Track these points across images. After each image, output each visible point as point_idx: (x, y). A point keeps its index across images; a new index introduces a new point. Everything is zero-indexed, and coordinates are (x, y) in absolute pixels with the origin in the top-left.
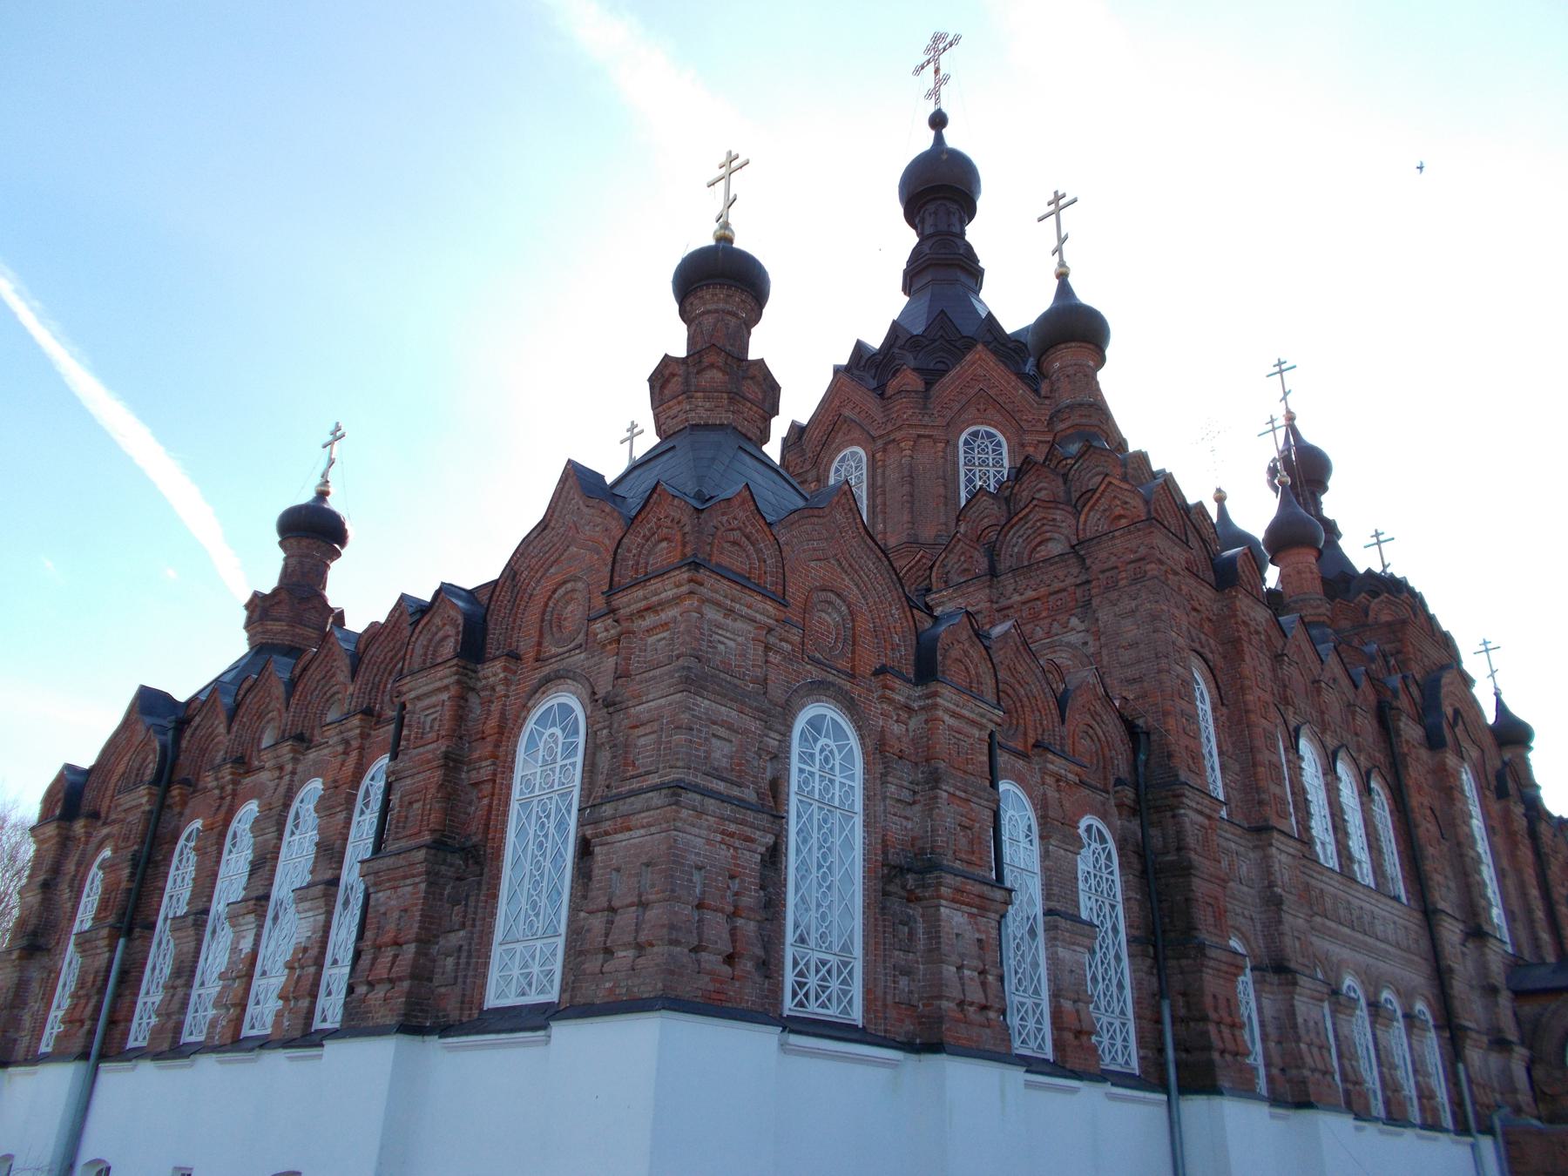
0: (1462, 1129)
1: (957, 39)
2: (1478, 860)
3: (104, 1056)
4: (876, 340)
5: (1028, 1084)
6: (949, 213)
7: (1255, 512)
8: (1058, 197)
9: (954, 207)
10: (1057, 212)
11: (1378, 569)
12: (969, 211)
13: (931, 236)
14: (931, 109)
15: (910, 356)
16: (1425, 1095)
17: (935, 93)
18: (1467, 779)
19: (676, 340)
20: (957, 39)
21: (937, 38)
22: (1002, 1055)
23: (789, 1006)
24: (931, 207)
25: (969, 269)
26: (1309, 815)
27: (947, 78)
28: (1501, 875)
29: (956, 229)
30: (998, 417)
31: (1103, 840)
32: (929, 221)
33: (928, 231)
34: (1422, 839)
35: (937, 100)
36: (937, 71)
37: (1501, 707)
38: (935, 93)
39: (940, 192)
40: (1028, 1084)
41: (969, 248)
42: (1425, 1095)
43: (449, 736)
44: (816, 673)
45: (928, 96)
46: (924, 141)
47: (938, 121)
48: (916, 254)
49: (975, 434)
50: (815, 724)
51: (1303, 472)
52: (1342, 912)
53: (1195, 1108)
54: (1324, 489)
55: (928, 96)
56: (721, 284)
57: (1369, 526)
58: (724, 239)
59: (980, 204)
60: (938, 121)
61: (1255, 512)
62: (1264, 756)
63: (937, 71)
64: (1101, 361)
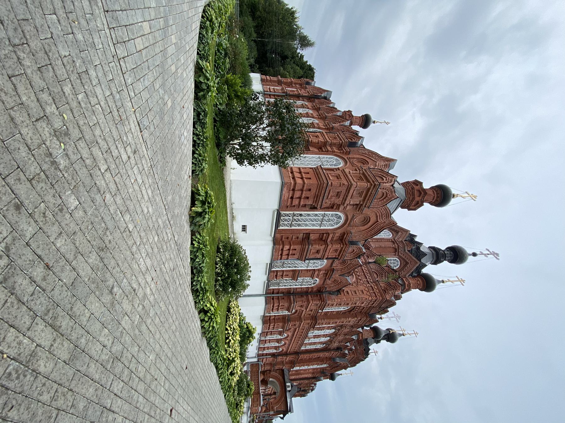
0: (259, 355)
1: (498, 259)
2: (308, 365)
4: (417, 239)
5: (267, 264)
7: (384, 323)
10: (459, 280)
11: (247, 292)
12: (452, 261)
14: (478, 253)
15: (415, 247)
16: (264, 349)
17: (482, 254)
18: (325, 366)
19: (426, 186)
20: (498, 259)
21: (497, 254)
22: (273, 260)
23: (282, 212)
25: (436, 262)
26: (318, 330)
28: (305, 370)
29: (447, 259)
30: (402, 266)
31: (314, 284)
32: (448, 252)
33: (446, 252)
34: (313, 355)
37: (339, 375)
38: (482, 254)
39: (456, 255)
40: (267, 264)
41: (442, 261)
42: (264, 349)
44: (350, 218)
46: (469, 251)
47: (474, 255)
48: (440, 250)
50: (340, 217)
51: (391, 337)
53: (262, 299)
54: (387, 341)
55: (481, 252)
56: (441, 196)
57: (379, 349)
58: (454, 196)
59: (453, 264)
60: (474, 255)
61: (384, 323)
64: (421, 290)
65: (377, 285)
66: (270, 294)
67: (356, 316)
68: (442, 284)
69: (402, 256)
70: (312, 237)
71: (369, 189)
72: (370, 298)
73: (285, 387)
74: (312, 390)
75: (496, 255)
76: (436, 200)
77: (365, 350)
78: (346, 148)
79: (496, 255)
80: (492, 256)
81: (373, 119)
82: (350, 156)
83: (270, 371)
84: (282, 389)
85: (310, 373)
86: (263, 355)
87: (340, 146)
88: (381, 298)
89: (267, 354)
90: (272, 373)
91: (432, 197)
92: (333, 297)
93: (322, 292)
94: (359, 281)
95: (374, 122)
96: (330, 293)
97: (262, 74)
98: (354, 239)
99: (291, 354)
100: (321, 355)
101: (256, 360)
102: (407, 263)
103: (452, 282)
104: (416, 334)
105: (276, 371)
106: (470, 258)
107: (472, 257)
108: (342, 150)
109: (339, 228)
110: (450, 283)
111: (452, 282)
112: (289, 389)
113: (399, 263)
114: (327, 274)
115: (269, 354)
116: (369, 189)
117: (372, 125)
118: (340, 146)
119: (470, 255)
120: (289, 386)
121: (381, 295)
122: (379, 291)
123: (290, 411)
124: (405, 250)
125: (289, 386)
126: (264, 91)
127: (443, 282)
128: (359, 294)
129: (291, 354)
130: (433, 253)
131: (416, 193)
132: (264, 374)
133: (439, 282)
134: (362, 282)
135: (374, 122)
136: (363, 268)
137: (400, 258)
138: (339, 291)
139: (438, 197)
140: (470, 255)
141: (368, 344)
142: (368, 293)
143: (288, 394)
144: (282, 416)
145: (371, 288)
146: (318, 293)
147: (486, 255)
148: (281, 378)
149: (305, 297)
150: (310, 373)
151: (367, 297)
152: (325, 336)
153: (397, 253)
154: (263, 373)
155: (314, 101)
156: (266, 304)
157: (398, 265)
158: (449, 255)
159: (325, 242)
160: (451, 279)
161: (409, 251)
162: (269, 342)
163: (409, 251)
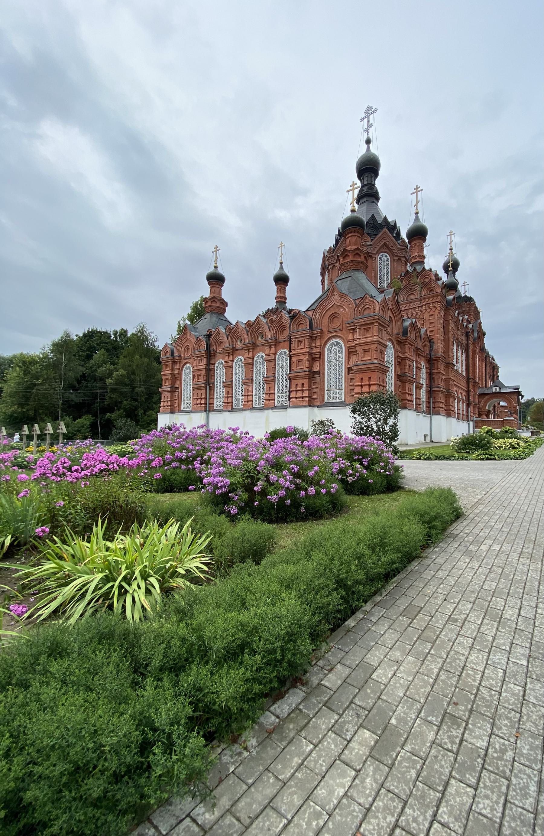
0: (467, 420)
3: (210, 411)
6: (372, 177)
8: (417, 188)
9: (373, 175)
10: (417, 192)
12: (376, 175)
13: (366, 185)
14: (365, 137)
17: (367, 130)
24: (367, 174)
27: (372, 125)
30: (388, 251)
32: (366, 179)
35: (368, 134)
36: (368, 121)
38: (367, 130)
43: (466, 296)
45: (365, 131)
47: (368, 142)
49: (382, 255)
51: (452, 267)
52: (339, 616)
53: (435, 418)
60: (368, 142)
62: (451, 347)
63: (368, 121)
65: (425, 299)
66: (430, 410)
67: (448, 321)
68: (420, 215)
69: (376, 250)
70: (399, 373)
71: (379, 324)
72: (439, 308)
73: (495, 393)
74: (493, 359)
75: (370, 111)
76: (360, 234)
77: (466, 302)
78: (315, 332)
79: (370, 111)
80: (371, 117)
81: (212, 270)
82: (325, 330)
83: (479, 408)
84: (497, 396)
85: (482, 364)
86: (467, 416)
87: (312, 338)
88: (439, 297)
89: (467, 412)
90: (481, 406)
91: (358, 239)
92: (435, 347)
93: (430, 358)
94: (418, 316)
95: (216, 267)
96: (431, 350)
97: (159, 412)
98: (401, 330)
99: (468, 387)
100: (471, 354)
101: (471, 423)
102: (385, 244)
103: (417, 202)
104: (417, 190)
105: (480, 402)
106: (374, 150)
107: (371, 145)
108: (316, 337)
109: (394, 347)
110: (419, 205)
111: (417, 202)
112: (498, 390)
113: (384, 254)
114: (419, 355)
115: (467, 409)
116: (379, 324)
117: (220, 271)
118: (312, 338)
119: (368, 148)
120: (496, 389)
121: (436, 296)
122: (431, 297)
123: (518, 389)
124: (371, 245)
125: (496, 389)
126: (206, 411)
127: (417, 213)
128: (434, 319)
129: (468, 387)
130: (367, 201)
131: (357, 259)
132: (482, 415)
133: (417, 219)
134: (419, 314)
135: (216, 267)
136: (403, 309)
137: (378, 252)
138: (430, 341)
139: (358, 232)
140: (368, 148)
141: (460, 297)
142: (434, 310)
143: (502, 391)
144: (520, 397)
145: (427, 306)
146: (431, 362)
147: (370, 126)
148: (487, 397)
149: (434, 376)
150: (482, 364)
151: (437, 311)
152: (457, 350)
153: (373, 256)
154: (480, 415)
155: (214, 351)
156: (439, 414)
157: (386, 256)
158: (369, 179)
159: (402, 359)
160: (414, 203)
161: (372, 240)
162: (226, 367)
163: (372, 240)
